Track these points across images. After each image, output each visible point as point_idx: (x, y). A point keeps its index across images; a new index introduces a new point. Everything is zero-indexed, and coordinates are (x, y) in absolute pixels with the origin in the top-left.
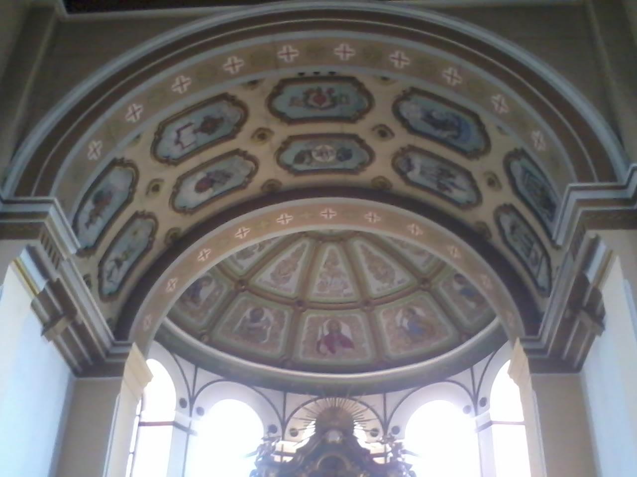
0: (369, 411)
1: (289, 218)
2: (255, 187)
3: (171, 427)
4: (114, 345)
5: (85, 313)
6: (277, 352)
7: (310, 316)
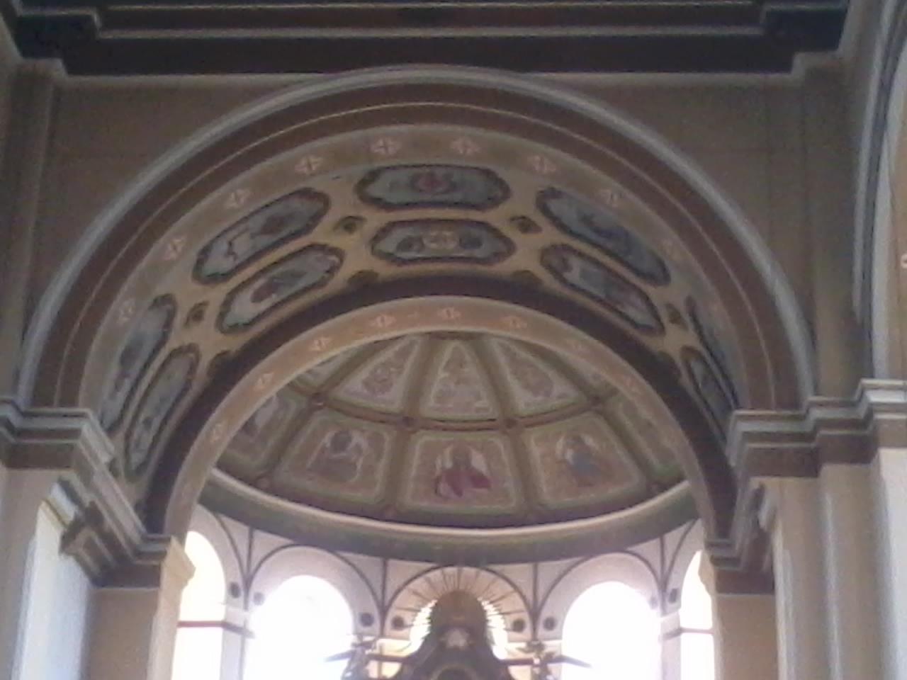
0: (501, 581)
1: (389, 320)
2: (339, 281)
3: (219, 631)
4: (146, 540)
5: (112, 514)
6: (372, 495)
7: (422, 440)
